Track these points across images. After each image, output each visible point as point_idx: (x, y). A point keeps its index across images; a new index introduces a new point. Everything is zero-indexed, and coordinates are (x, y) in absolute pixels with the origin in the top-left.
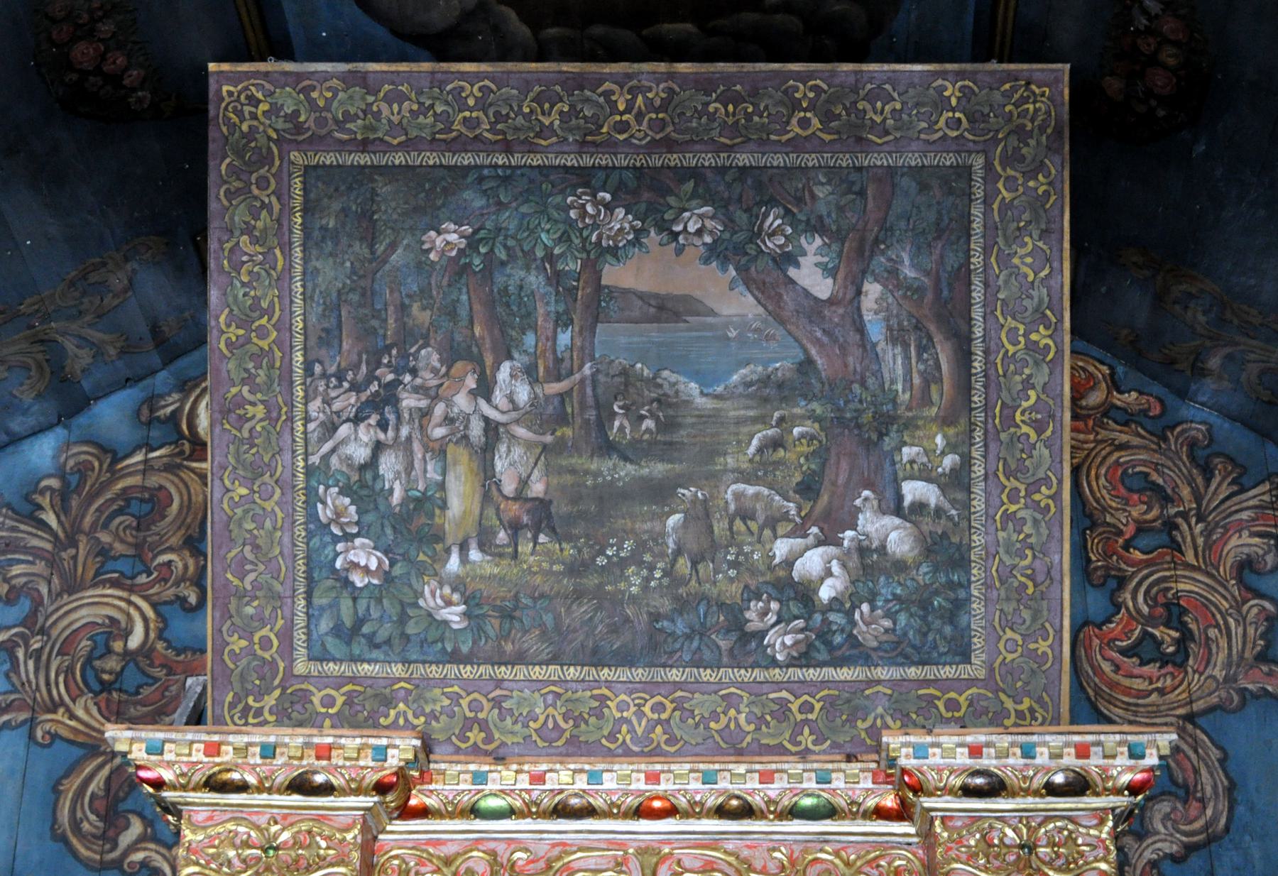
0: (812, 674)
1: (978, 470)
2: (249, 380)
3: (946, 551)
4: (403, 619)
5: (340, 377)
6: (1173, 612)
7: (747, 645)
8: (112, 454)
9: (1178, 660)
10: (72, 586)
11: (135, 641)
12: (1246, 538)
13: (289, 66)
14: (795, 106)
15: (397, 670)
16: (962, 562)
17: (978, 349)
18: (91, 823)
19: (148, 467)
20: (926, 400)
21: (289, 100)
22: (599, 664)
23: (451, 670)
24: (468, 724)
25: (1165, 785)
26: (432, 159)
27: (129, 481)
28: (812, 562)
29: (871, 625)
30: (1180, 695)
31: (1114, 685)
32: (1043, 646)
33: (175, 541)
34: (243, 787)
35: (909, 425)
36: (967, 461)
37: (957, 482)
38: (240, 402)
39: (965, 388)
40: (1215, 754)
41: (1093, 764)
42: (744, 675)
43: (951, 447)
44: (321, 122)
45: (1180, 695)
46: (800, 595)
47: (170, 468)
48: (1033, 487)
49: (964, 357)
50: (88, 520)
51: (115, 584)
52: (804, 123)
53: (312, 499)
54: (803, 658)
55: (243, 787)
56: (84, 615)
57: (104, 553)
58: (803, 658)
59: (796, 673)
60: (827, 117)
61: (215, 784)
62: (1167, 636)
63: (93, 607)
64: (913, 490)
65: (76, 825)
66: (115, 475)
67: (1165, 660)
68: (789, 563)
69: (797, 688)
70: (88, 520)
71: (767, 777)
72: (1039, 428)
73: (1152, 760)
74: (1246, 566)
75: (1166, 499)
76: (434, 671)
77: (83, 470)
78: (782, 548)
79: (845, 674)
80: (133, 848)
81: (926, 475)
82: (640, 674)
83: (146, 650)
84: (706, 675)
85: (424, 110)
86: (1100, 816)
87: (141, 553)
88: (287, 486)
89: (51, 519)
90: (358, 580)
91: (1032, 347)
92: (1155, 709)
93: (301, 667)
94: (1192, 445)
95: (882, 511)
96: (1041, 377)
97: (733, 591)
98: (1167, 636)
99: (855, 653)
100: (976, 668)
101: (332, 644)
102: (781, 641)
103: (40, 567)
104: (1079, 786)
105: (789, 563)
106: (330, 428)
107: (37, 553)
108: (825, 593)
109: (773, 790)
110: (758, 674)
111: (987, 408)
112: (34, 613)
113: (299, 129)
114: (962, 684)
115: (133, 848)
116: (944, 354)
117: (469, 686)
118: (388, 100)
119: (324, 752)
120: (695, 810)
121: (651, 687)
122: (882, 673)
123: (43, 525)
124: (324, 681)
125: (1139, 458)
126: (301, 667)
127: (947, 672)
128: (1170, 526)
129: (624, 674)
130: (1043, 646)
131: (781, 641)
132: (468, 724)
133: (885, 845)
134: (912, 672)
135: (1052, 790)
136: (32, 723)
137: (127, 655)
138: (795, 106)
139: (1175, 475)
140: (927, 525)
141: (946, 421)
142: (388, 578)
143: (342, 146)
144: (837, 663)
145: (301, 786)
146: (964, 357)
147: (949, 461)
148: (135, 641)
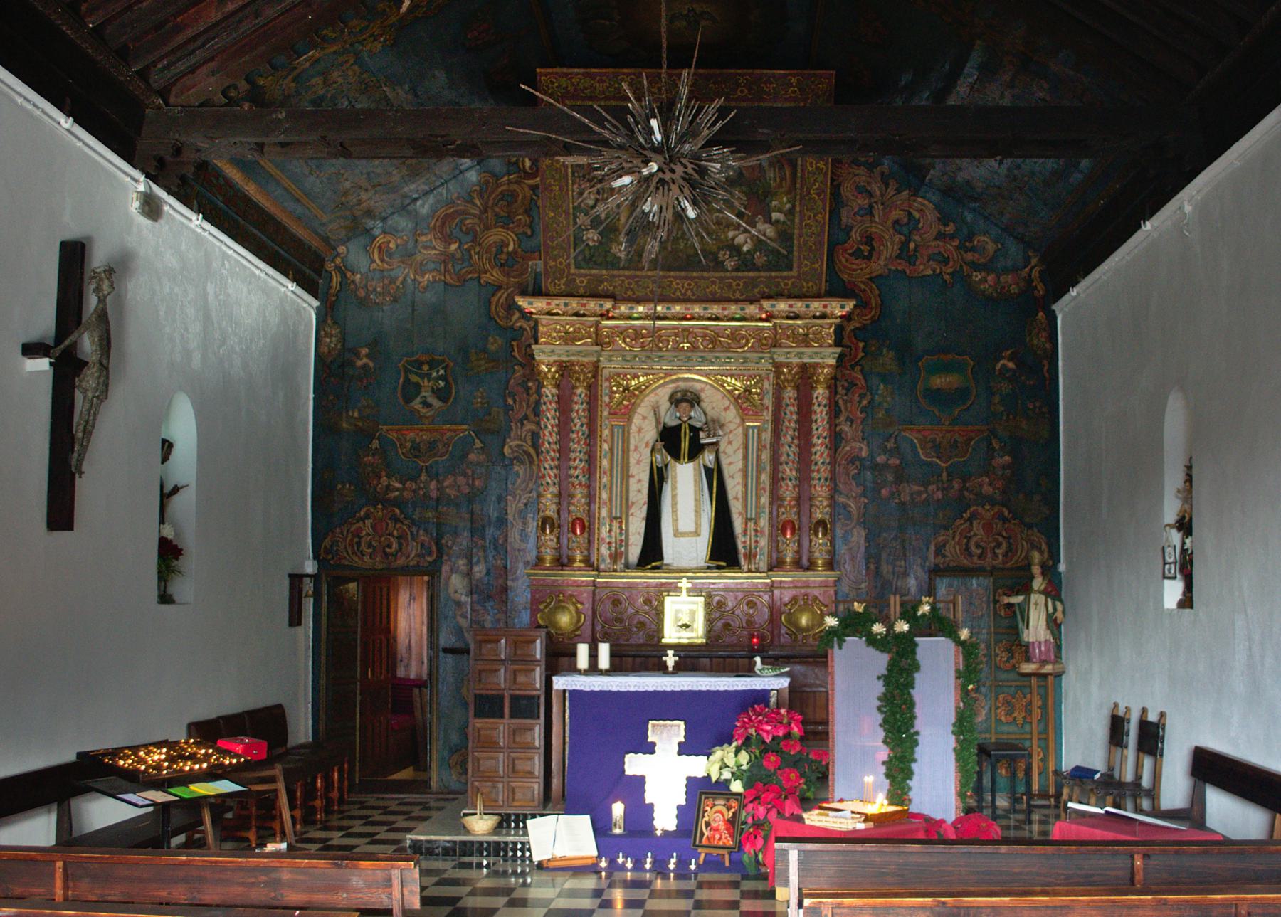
0: (740, 274)
1: (798, 209)
2: (553, 177)
3: (785, 236)
4: (606, 257)
5: (584, 177)
6: (869, 240)
7: (719, 265)
8: (496, 177)
9: (869, 258)
10: (488, 228)
11: (511, 248)
12: (898, 212)
13: (565, 70)
14: (739, 85)
15: (604, 272)
16: (791, 239)
17: (799, 169)
18: (502, 313)
19: (509, 182)
20: (780, 186)
21: (564, 82)
22: (669, 270)
23: (621, 272)
24: (627, 289)
25: (847, 318)
26: (614, 103)
27: (504, 187)
28: (741, 239)
29: (760, 259)
30: (867, 271)
31: (845, 267)
32: (816, 266)
33: (521, 211)
34: (557, 314)
35: (775, 194)
36: (794, 206)
37: (790, 213)
38: (551, 185)
39: (794, 182)
40: (877, 292)
41: (828, 310)
42: (717, 274)
43: (789, 201)
44: (575, 90)
45: (867, 271)
46: (735, 250)
47: (518, 183)
48: (816, 215)
49: (794, 175)
50: (490, 203)
51: (502, 227)
52: (742, 91)
53: (575, 217)
54: (737, 269)
55: (557, 314)
56: (493, 239)
57: (497, 215)
58: (737, 269)
59: (735, 274)
60: (750, 89)
61: (549, 313)
62: (865, 248)
63: (497, 235)
64: (775, 216)
65: (497, 314)
66: (498, 186)
67: (864, 258)
68: (733, 239)
69: (734, 279)
70: (490, 203)
71: (724, 309)
72: (819, 195)
73: (847, 309)
74: (896, 222)
75: (871, 195)
76: (615, 272)
77: (487, 182)
78: (731, 234)
79: (751, 274)
80: (516, 321)
81: (780, 211)
82: (683, 274)
83: (515, 252)
84: (705, 274)
85: (611, 86)
86: (830, 325)
87: (510, 218)
88: (567, 213)
89: (478, 203)
90: (591, 244)
91: (817, 168)
92: (790, 393)
93: (573, 271)
94: (882, 174)
95: (765, 222)
96: (820, 179)
97: (715, 248)
98: (865, 248)
99: (755, 268)
100: (794, 273)
101: (582, 263)
102: (730, 264)
103: (476, 220)
104: (823, 316)
105: (733, 239)
106: (581, 194)
107: (475, 215)
108: (745, 249)
109: (726, 313)
110: (722, 274)
111: (802, 188)
112: (475, 237)
113: (568, 92)
114: (788, 278)
115: (516, 321)
116: (788, 172)
117: (627, 277)
118: (599, 82)
119: (584, 305)
120: (700, 318)
121: (686, 278)
122: (763, 274)
123: (474, 204)
124: (580, 275)
125: (862, 180)
126: (573, 271)
127: (785, 274)
128: (871, 206)
129: (678, 274)
130: (816, 266)
131: (730, 264)
132: (627, 289)
133: (762, 329)
134: (773, 274)
135: (815, 317)
136: (479, 278)
137: (508, 253)
138: (739, 85)
139: (876, 188)
140: (780, 226)
141: (788, 192)
142: (601, 243)
143: (583, 99)
144: (749, 271)
145: (577, 314)
146: (794, 175)
147: (788, 206)
148: (511, 248)
